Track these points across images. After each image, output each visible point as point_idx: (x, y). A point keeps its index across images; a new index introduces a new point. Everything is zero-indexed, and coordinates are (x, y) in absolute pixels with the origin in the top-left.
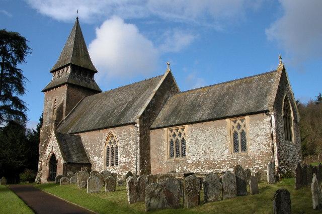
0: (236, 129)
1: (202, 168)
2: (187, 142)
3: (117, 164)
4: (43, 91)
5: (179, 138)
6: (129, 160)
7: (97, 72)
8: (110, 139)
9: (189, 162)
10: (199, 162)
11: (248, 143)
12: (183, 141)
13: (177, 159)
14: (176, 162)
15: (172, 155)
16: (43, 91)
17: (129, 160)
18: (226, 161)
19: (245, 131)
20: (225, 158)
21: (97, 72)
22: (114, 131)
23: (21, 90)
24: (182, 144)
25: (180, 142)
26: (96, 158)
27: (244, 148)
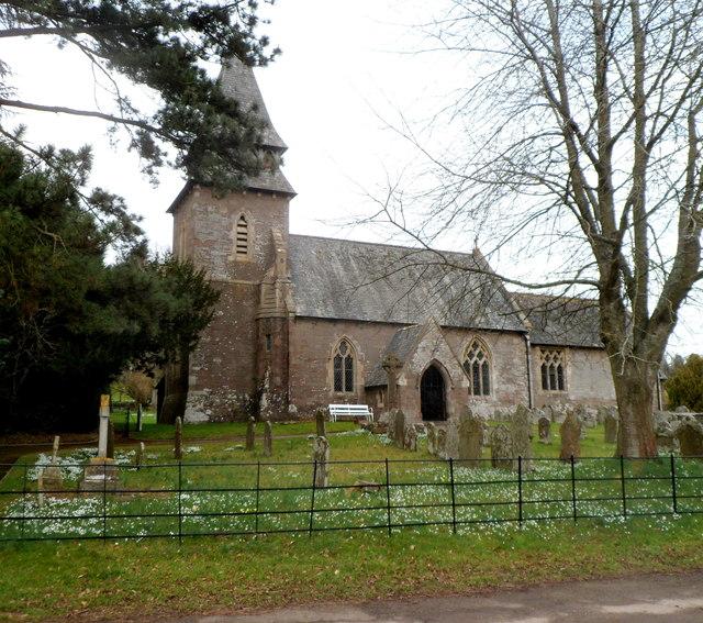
0: (544, 361)
3: (486, 392)
6: (512, 388)
9: (572, 398)
13: (553, 392)
15: (545, 386)
17: (512, 388)
25: (343, 361)
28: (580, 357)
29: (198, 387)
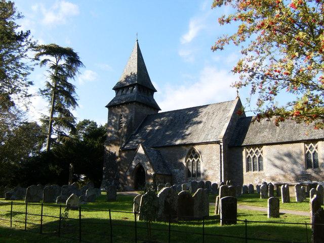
4: (106, 107)
7: (156, 91)
8: (192, 154)
14: (255, 175)
16: (106, 107)
21: (156, 91)
26: (175, 170)
29: (105, 178)
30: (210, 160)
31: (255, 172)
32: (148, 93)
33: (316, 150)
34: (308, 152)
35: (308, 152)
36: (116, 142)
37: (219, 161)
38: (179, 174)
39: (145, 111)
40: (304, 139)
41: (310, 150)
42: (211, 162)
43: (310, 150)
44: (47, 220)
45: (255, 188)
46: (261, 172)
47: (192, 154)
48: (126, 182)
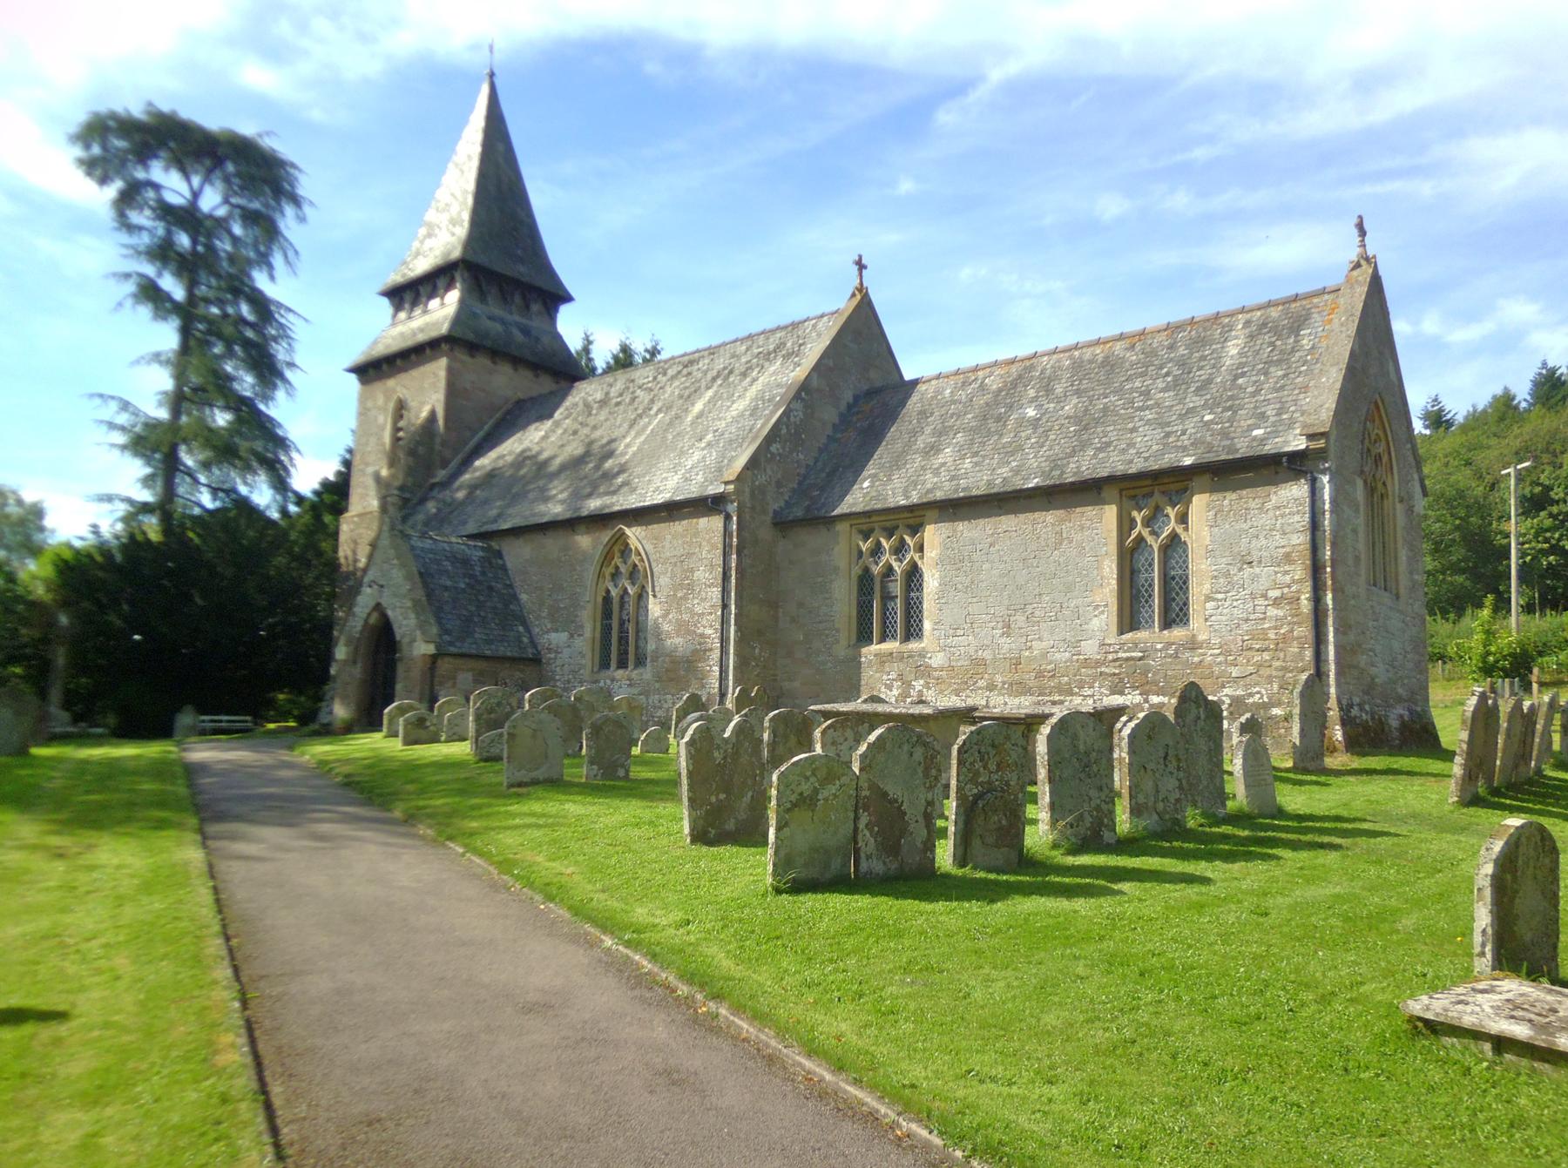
1: (991, 687)
2: (931, 582)
5: (895, 565)
8: (617, 561)
9: (937, 660)
10: (982, 663)
11: (1198, 589)
12: (914, 574)
18: (1098, 663)
19: (1183, 536)
20: (1090, 648)
21: (568, 298)
22: (635, 535)
23: (269, 371)
24: (626, 653)
26: (553, 636)
27: (1174, 614)
28: (970, 531)
30: (686, 586)
31: (890, 646)
32: (527, 307)
33: (1179, 530)
34: (1140, 539)
35: (1140, 539)
36: (185, 470)
37: (715, 593)
38: (566, 652)
39: (506, 382)
40: (1120, 468)
41: (1146, 533)
42: (685, 598)
43: (1146, 533)
44: (268, 513)
45: (1031, 789)
46: (914, 645)
47: (617, 561)
48: (178, 292)
